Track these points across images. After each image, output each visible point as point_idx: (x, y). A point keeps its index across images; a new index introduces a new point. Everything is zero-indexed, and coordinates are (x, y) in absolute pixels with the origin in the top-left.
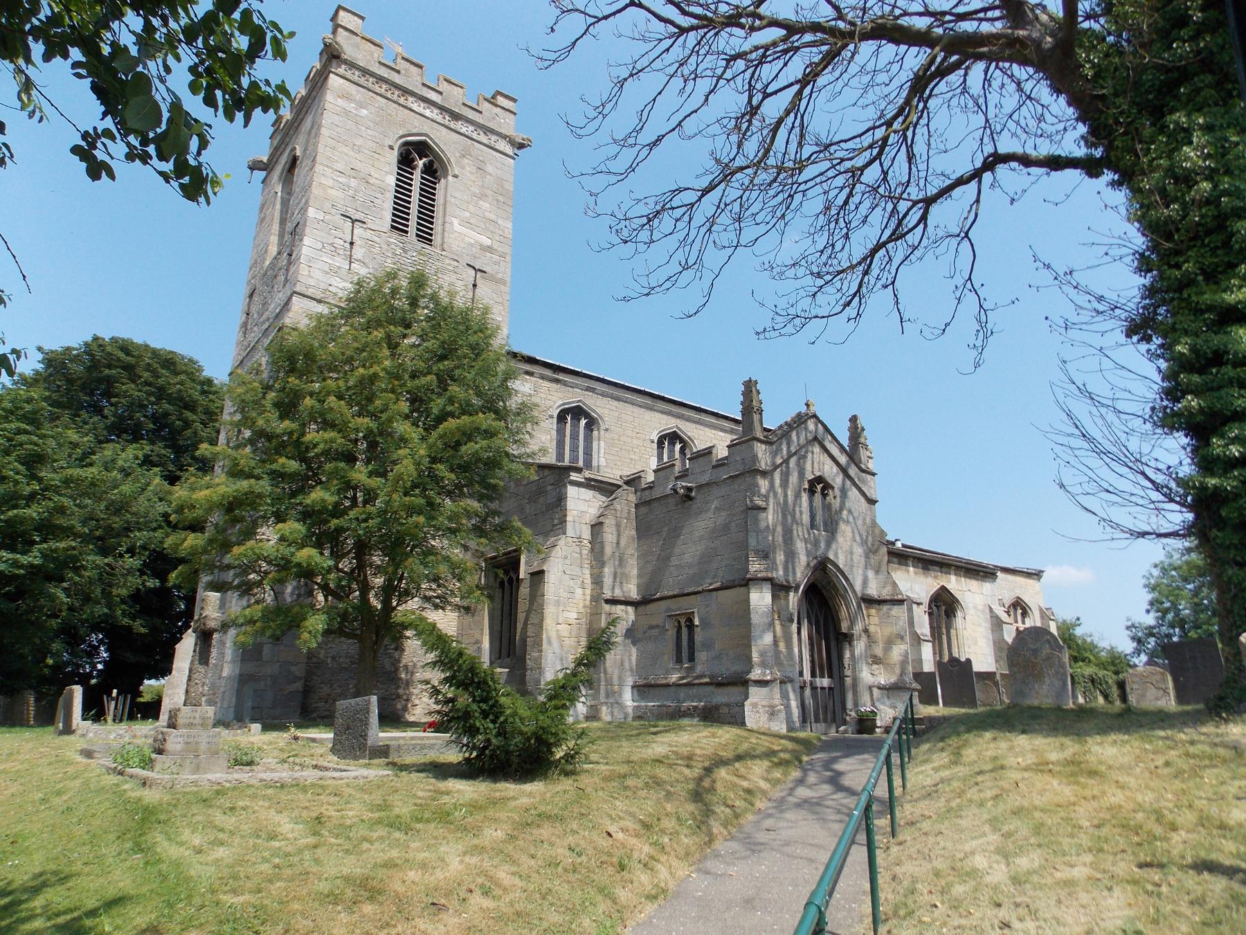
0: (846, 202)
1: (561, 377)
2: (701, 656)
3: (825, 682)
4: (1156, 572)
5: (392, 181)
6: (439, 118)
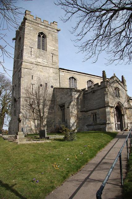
0: (119, 39)
1: (69, 72)
3: (119, 123)
5: (37, 40)
6: (44, 28)
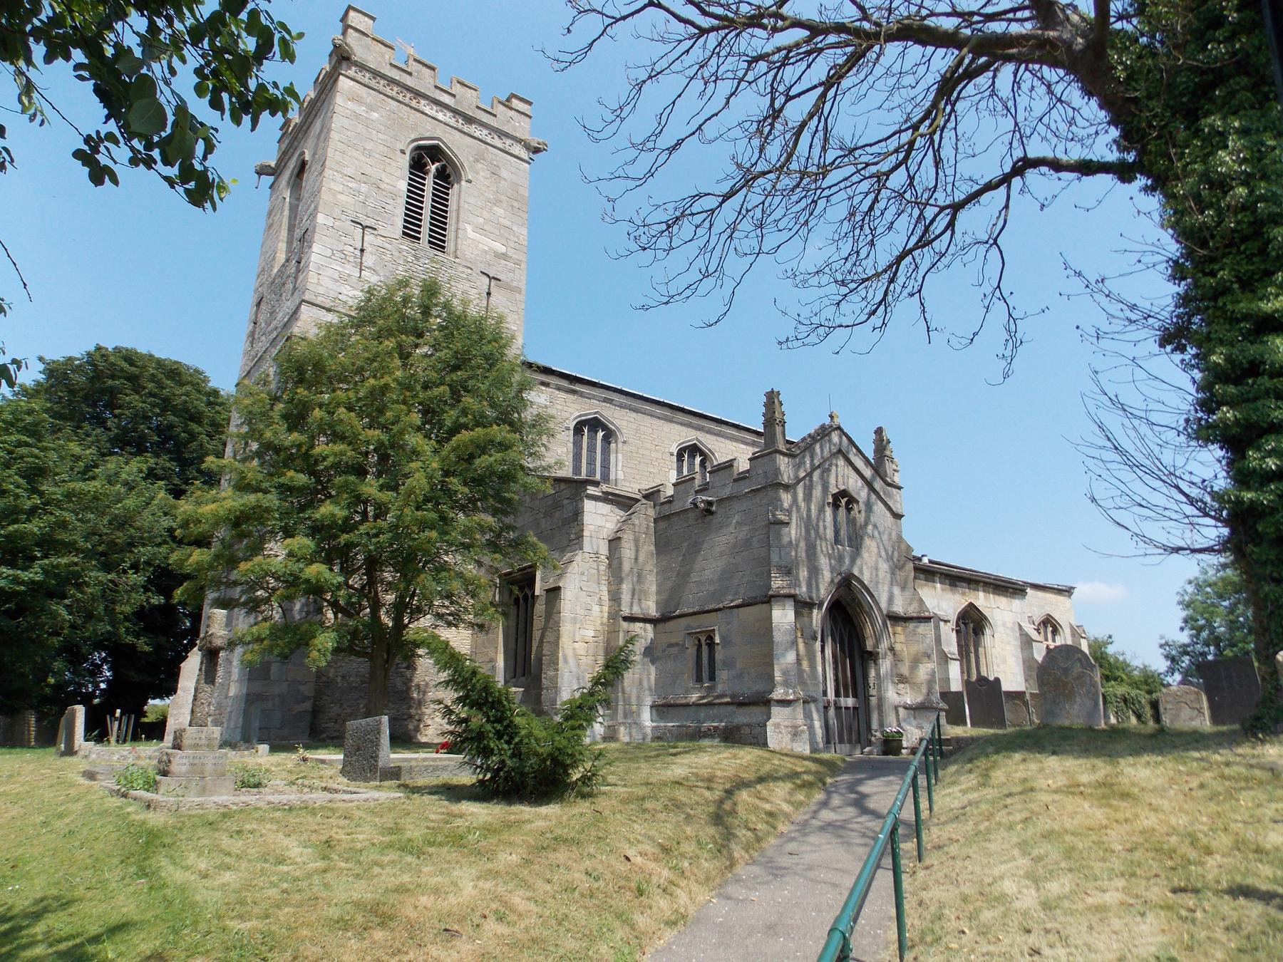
0: (871, 208)
1: (577, 387)
2: (722, 675)
3: (850, 702)
4: (1190, 589)
5: (403, 186)
6: (452, 122)
